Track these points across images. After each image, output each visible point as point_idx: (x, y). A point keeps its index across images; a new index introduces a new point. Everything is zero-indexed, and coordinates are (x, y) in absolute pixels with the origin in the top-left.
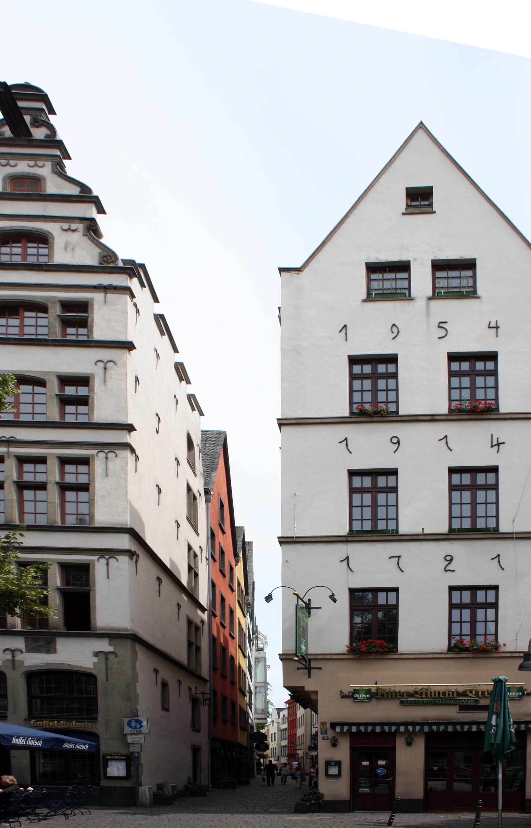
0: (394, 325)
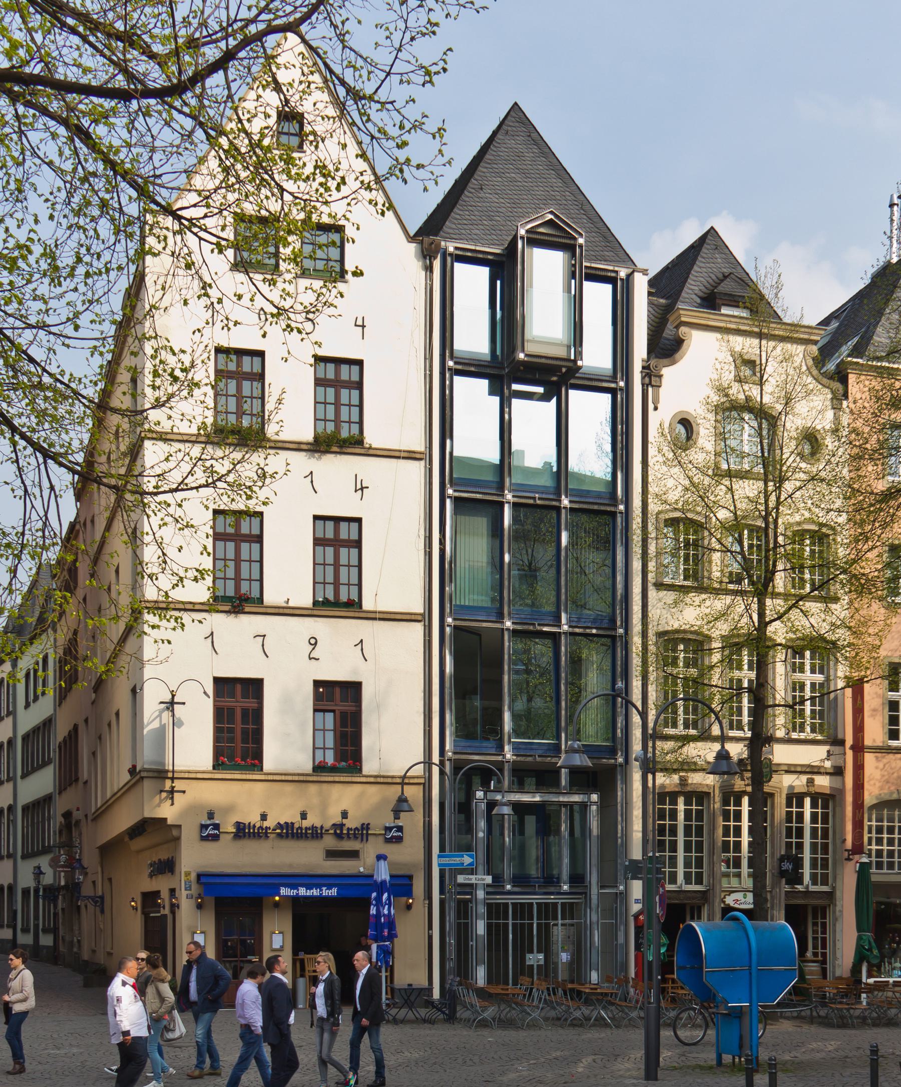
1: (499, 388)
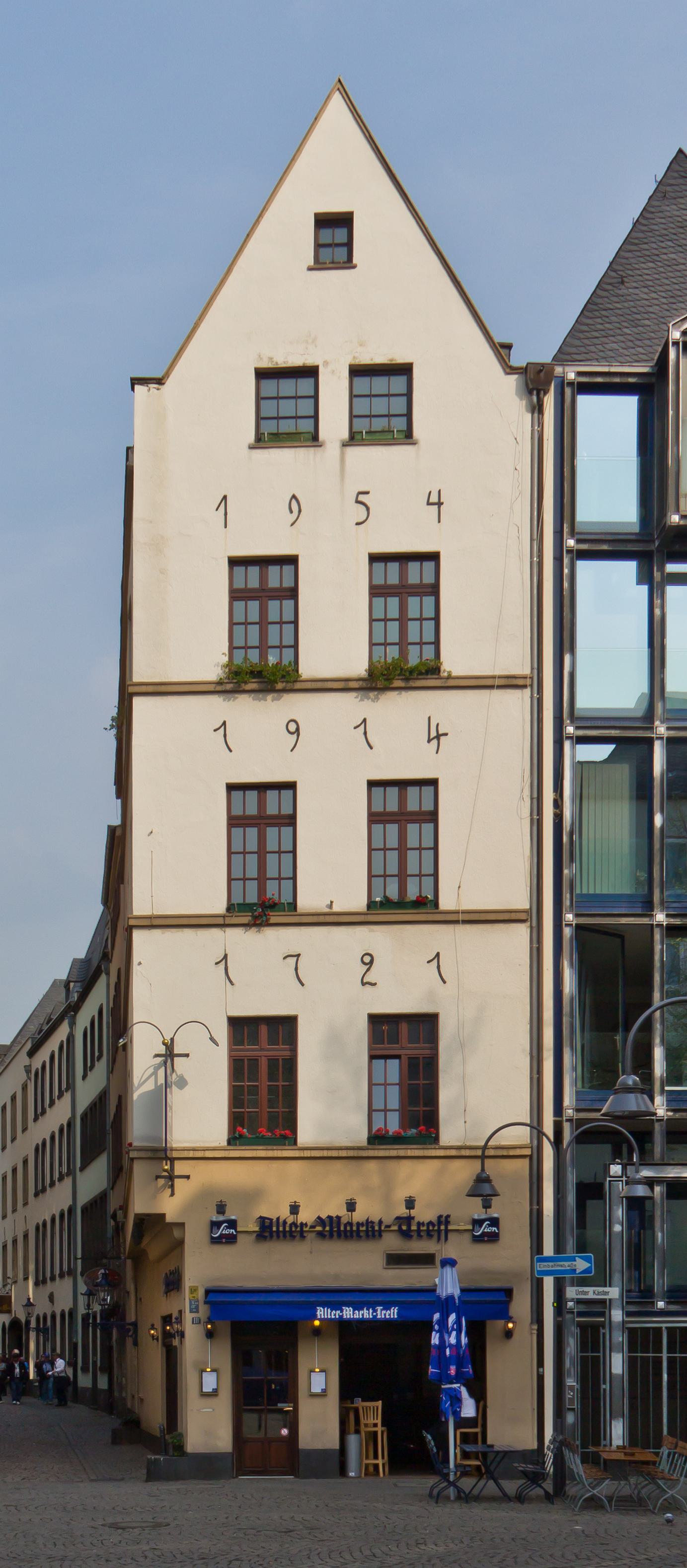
0: (294, 497)
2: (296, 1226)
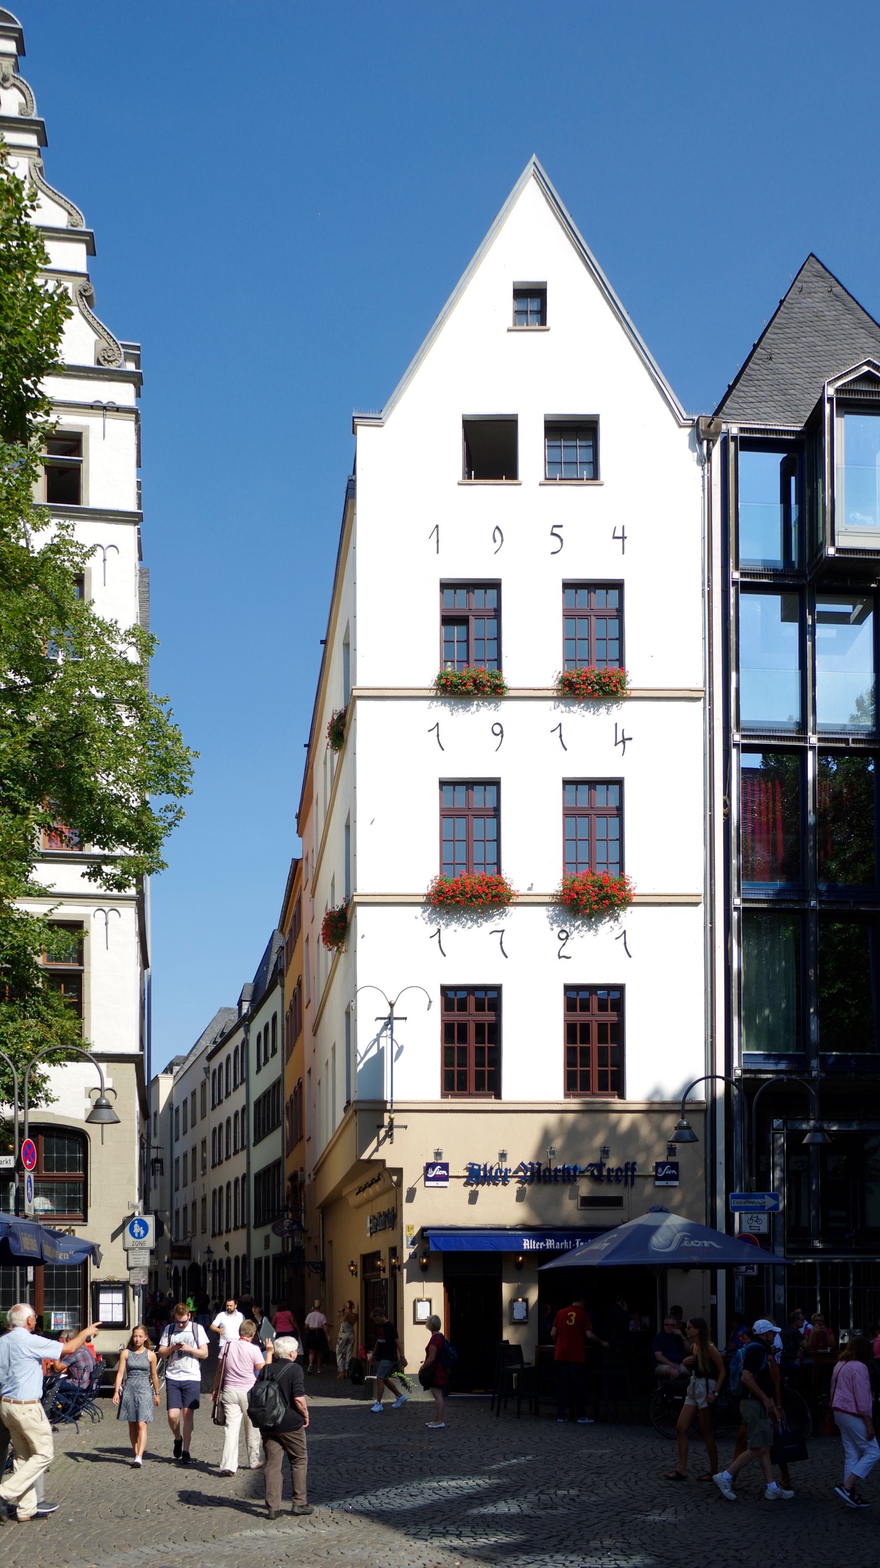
0: (497, 528)
1: (798, 611)
2: (501, 1172)
